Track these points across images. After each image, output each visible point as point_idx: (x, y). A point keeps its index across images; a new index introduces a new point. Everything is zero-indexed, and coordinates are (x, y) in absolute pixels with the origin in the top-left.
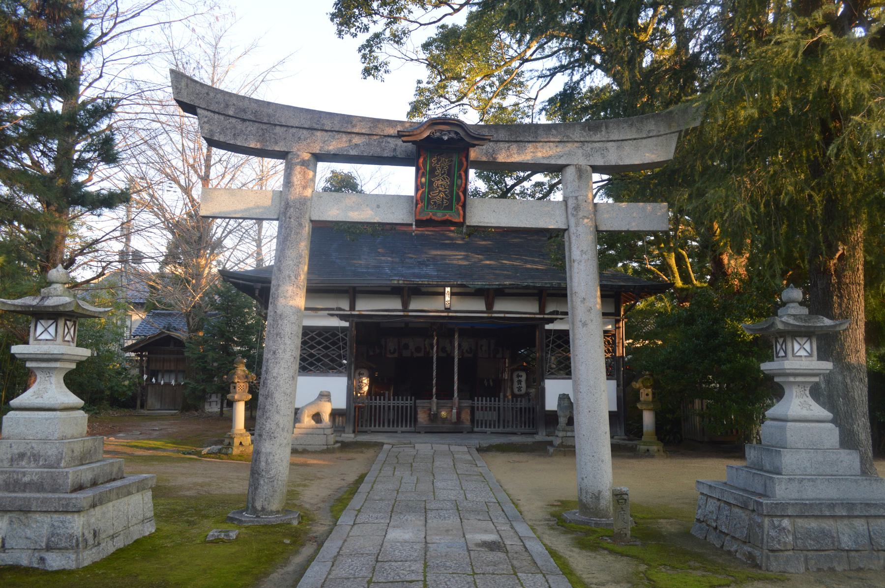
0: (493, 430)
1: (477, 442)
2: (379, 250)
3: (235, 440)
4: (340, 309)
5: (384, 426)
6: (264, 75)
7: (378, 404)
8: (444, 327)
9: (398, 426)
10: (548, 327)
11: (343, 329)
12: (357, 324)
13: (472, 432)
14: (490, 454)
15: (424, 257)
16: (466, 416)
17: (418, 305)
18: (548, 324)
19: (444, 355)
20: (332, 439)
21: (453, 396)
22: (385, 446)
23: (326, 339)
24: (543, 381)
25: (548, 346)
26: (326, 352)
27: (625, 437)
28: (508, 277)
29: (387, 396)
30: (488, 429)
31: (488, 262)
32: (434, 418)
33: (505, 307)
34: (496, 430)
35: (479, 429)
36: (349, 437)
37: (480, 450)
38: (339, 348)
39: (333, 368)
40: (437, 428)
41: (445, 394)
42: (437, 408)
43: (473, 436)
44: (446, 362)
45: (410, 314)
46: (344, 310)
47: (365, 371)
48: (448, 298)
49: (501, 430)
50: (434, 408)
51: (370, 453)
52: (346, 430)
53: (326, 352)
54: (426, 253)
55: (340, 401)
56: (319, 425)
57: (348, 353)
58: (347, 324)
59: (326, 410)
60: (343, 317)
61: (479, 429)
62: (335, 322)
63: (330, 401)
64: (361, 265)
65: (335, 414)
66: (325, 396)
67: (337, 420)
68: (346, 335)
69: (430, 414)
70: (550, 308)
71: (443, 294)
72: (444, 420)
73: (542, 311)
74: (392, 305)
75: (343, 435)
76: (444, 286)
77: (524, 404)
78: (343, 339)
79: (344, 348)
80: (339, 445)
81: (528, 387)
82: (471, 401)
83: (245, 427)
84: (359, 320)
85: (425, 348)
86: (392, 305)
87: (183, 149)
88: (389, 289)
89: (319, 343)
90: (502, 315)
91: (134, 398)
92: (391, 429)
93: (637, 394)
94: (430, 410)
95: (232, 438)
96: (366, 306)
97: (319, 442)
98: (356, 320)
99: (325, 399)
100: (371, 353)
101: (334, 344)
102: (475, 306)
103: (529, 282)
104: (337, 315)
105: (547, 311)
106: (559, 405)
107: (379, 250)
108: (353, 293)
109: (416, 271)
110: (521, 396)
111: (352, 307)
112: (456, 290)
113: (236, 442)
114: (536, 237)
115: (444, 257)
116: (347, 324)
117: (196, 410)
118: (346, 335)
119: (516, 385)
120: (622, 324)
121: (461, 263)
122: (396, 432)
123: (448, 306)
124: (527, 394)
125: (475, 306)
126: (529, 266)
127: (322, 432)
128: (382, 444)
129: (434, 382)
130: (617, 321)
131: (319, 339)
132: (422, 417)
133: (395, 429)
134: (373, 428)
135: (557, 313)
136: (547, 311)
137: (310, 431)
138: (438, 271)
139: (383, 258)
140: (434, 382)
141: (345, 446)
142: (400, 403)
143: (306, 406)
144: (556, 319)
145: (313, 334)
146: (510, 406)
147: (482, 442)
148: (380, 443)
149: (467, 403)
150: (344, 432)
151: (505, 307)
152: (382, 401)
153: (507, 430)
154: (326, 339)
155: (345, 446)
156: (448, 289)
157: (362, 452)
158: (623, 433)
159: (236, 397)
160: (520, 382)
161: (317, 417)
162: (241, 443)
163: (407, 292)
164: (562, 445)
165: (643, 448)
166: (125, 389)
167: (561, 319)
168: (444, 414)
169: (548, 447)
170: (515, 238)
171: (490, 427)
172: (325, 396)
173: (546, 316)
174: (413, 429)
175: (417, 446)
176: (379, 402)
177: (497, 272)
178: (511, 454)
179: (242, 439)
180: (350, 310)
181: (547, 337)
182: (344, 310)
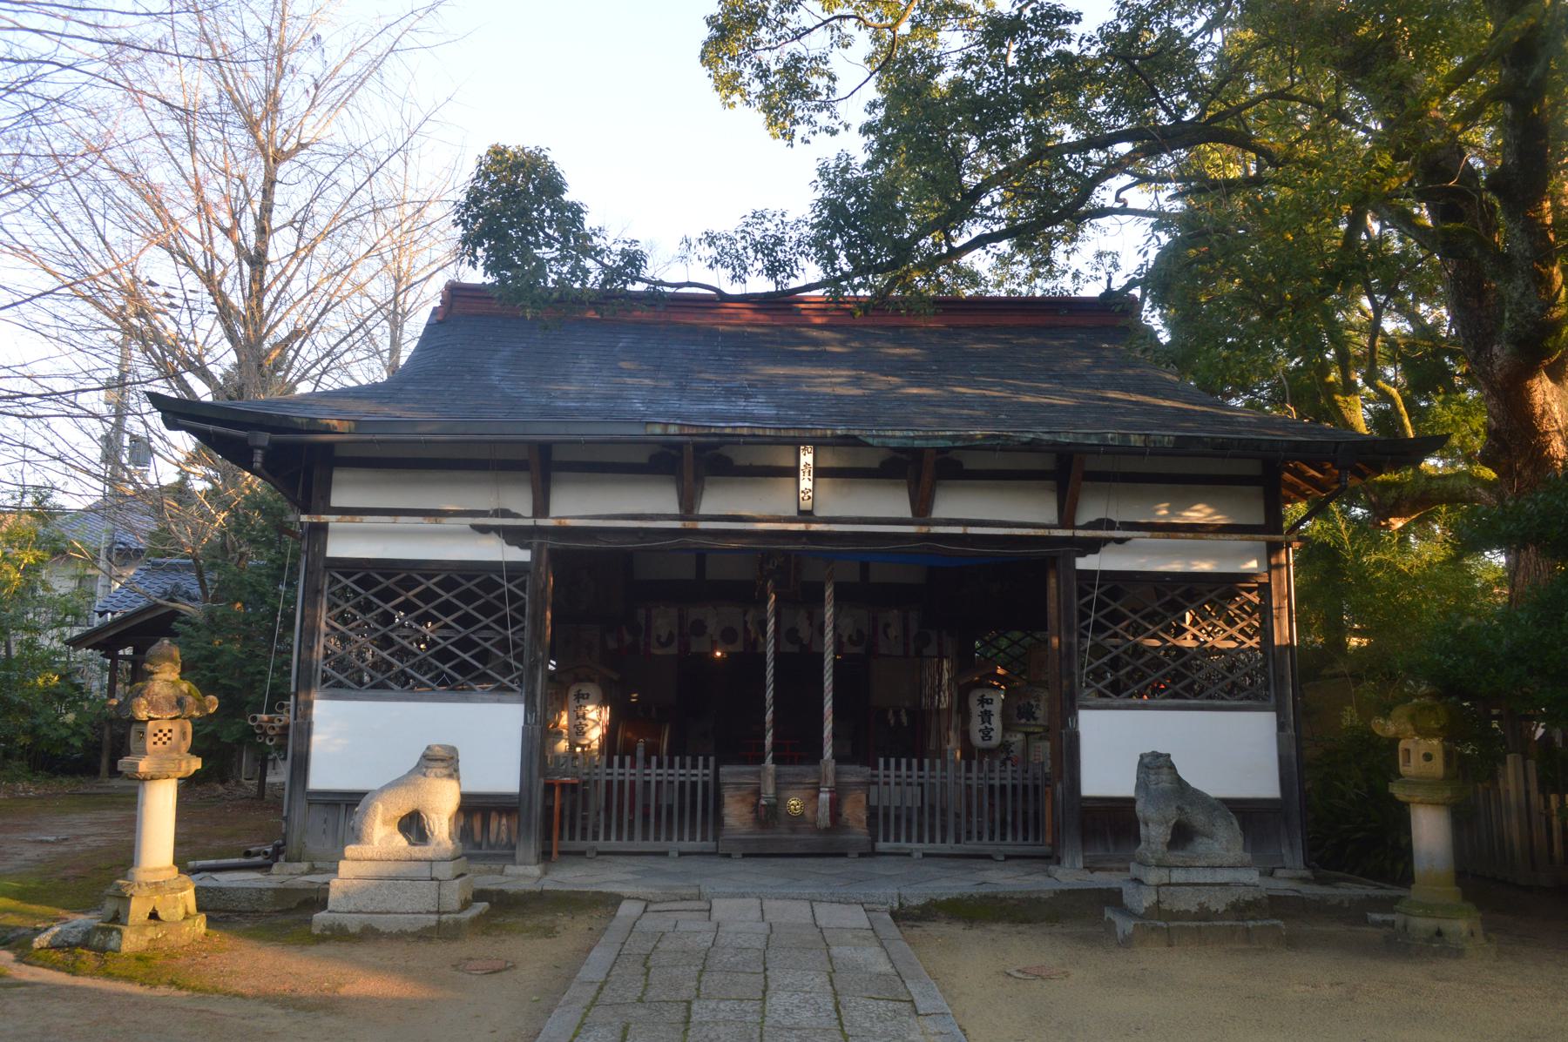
1: (892, 891)
2: (623, 364)
3: (135, 905)
4: (505, 513)
5: (631, 838)
6: (395, 31)
7: (616, 778)
8: (790, 562)
9: (669, 838)
10: (1084, 563)
11: (515, 569)
12: (554, 555)
13: (873, 853)
14: (933, 929)
15: (741, 379)
16: (854, 811)
17: (726, 504)
18: (1083, 555)
19: (795, 649)
20: (454, 894)
22: (628, 910)
23: (468, 597)
24: (1073, 714)
25: (1084, 616)
26: (464, 632)
27: (1307, 873)
28: (975, 422)
29: (640, 753)
30: (914, 845)
31: (915, 391)
32: (768, 815)
33: (964, 509)
34: (938, 847)
35: (890, 846)
36: (524, 875)
37: (903, 916)
38: (502, 622)
39: (483, 678)
40: (776, 843)
41: (799, 747)
42: (778, 789)
43: (877, 867)
44: (800, 669)
45: (702, 525)
46: (517, 516)
47: (592, 689)
48: (806, 483)
49: (949, 846)
50: (769, 790)
51: (573, 928)
52: (520, 853)
53: (464, 632)
54: (747, 372)
55: (499, 770)
56: (418, 851)
57: (527, 635)
58: (524, 556)
59: (442, 803)
60: (513, 536)
61: (890, 846)
62: (492, 550)
63: (454, 773)
64: (566, 393)
65: (474, 808)
66: (442, 760)
67: (494, 825)
68: (522, 587)
69: (756, 806)
70: (1089, 512)
71: (794, 472)
72: (796, 822)
73: (1066, 520)
74: (648, 504)
75: (510, 869)
76: (796, 444)
77: (1003, 776)
78: (514, 598)
79: (515, 622)
80: (483, 906)
81: (1006, 728)
82: (867, 770)
83: (175, 862)
84: (559, 544)
85: (746, 630)
86: (648, 504)
87: (197, 183)
88: (643, 458)
89: (447, 608)
90: (958, 530)
91: (94, 749)
92: (651, 845)
93: (1380, 758)
94: (758, 793)
95: (125, 900)
96: (579, 506)
97: (415, 905)
98: (550, 543)
99: (439, 769)
100: (612, 644)
101: (487, 610)
102: (883, 507)
103: (1040, 433)
104: (497, 530)
106: (1141, 785)
107: (623, 364)
108: (543, 465)
109: (719, 406)
110: (990, 751)
111: (541, 508)
112: (829, 461)
113: (138, 910)
114: (1032, 340)
115: (795, 380)
116: (524, 556)
117: (223, 782)
118: (522, 587)
119: (976, 725)
120: (1288, 557)
121: (840, 391)
122: (665, 854)
123: (806, 505)
124: (1005, 746)
125: (883, 507)
126: (1028, 399)
127: (424, 871)
128: (614, 901)
129: (769, 716)
130: (1273, 549)
131: (446, 596)
132: (736, 813)
133: (662, 845)
135: (1110, 525)
136: (1080, 521)
137: (390, 869)
138: (778, 406)
139: (629, 381)
140: (769, 716)
141: (503, 908)
142: (678, 774)
143: (382, 790)
144: (1107, 541)
145: (430, 583)
147: (905, 892)
148: (610, 895)
149: (856, 774)
150: (511, 858)
151: (964, 509)
152: (628, 770)
154: (468, 597)
155: (503, 908)
156: (807, 458)
157: (549, 932)
158: (1300, 863)
159: (144, 766)
160: (986, 716)
161: (413, 825)
162: (154, 916)
163: (696, 461)
164: (1156, 910)
165: (1422, 924)
166: (64, 732)
167: (1121, 541)
168: (794, 803)
169: (1108, 913)
170: (980, 340)
171: (920, 840)
172: (442, 760)
174: (710, 845)
175: (721, 907)
176: (628, 773)
177: (945, 410)
178: (998, 927)
179: (157, 901)
180: (536, 515)
181: (1082, 593)
182: (517, 516)
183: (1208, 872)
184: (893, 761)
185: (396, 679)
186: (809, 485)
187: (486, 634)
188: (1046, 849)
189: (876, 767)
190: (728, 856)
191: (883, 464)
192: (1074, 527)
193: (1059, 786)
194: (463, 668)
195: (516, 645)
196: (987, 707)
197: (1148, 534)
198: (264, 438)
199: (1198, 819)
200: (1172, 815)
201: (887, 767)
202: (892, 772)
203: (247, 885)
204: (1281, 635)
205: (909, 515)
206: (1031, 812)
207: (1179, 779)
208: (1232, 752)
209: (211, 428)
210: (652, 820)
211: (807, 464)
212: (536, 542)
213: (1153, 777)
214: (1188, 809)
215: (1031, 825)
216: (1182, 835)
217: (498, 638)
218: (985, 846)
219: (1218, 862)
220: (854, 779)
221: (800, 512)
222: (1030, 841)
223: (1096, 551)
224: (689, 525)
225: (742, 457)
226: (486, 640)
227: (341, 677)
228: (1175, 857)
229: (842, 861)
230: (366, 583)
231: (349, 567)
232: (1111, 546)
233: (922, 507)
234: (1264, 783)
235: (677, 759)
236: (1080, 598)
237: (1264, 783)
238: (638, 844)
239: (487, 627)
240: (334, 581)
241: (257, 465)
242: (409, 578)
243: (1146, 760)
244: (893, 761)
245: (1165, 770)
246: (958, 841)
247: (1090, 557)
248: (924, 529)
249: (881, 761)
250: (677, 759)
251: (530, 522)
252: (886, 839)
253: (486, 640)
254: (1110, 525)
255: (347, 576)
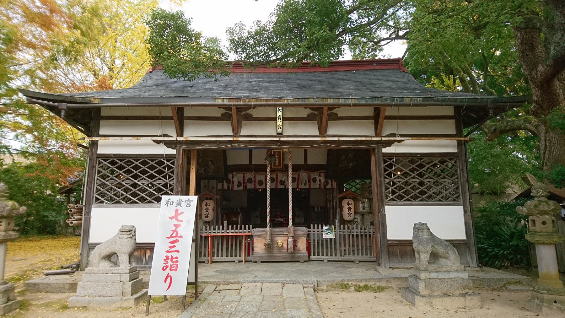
0: (329, 258)
5: (222, 256)
10: (385, 150)
11: (169, 157)
13: (310, 260)
16: (302, 245)
17: (250, 132)
21: (288, 224)
24: (382, 206)
30: (325, 257)
33: (339, 132)
41: (279, 221)
44: (279, 195)
45: (240, 139)
48: (279, 123)
49: (338, 258)
57: (175, 181)
58: (174, 152)
60: (169, 144)
62: (163, 150)
68: (173, 163)
79: (170, 177)
84: (187, 147)
86: (221, 132)
90: (336, 139)
96: (192, 133)
101: (160, 172)
102: (308, 131)
105: (385, 133)
116: (174, 152)
118: (173, 163)
123: (280, 131)
125: (308, 131)
132: (259, 246)
134: (216, 258)
135: (394, 135)
144: (395, 141)
146: (346, 234)
149: (304, 230)
153: (347, 257)
154: (152, 168)
160: (207, 209)
167: (399, 141)
171: (327, 255)
173: (383, 139)
183: (446, 274)
184: (316, 225)
185: (123, 199)
186: (281, 123)
187: (159, 181)
188: (375, 259)
189: (309, 228)
190: (256, 262)
191: (308, 115)
192: (381, 137)
193: (378, 235)
194: (134, 195)
195: (170, 185)
196: (208, 207)
197: (410, 138)
198: (64, 106)
199: (441, 250)
200: (429, 248)
201: (314, 228)
202: (316, 230)
203: (56, 282)
204: (256, 232)
205: (318, 134)
206: (368, 245)
207: (431, 233)
208: (448, 221)
209: (43, 102)
210: (230, 249)
211: (279, 116)
212: (178, 146)
213: (420, 233)
214: (436, 246)
215: (369, 249)
216: (434, 256)
217: (164, 183)
218: (351, 258)
219: (450, 269)
220: (302, 233)
221: (278, 134)
222: (369, 255)
223: (390, 146)
224: (235, 139)
225: (255, 113)
226: (159, 184)
227: (135, 199)
228: (432, 267)
229: (297, 264)
230: (113, 163)
231: (106, 157)
232: (396, 143)
233: (323, 131)
234: (461, 235)
235: (230, 226)
236: (384, 163)
237: (461, 235)
238: (224, 258)
239: (159, 179)
240: (100, 163)
241: (63, 116)
242: (129, 161)
243: (417, 226)
244: (316, 225)
245: (426, 230)
246: (341, 256)
247: (388, 148)
248: (323, 139)
249: (312, 225)
250: (230, 226)
251: (174, 139)
252: (314, 255)
253: (159, 184)
254: (394, 135)
255: (105, 161)
